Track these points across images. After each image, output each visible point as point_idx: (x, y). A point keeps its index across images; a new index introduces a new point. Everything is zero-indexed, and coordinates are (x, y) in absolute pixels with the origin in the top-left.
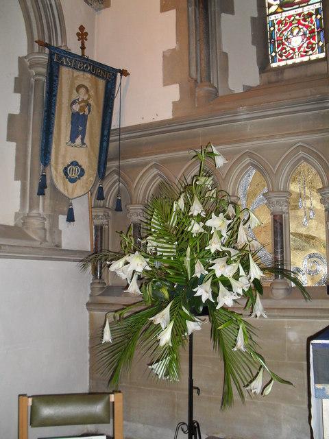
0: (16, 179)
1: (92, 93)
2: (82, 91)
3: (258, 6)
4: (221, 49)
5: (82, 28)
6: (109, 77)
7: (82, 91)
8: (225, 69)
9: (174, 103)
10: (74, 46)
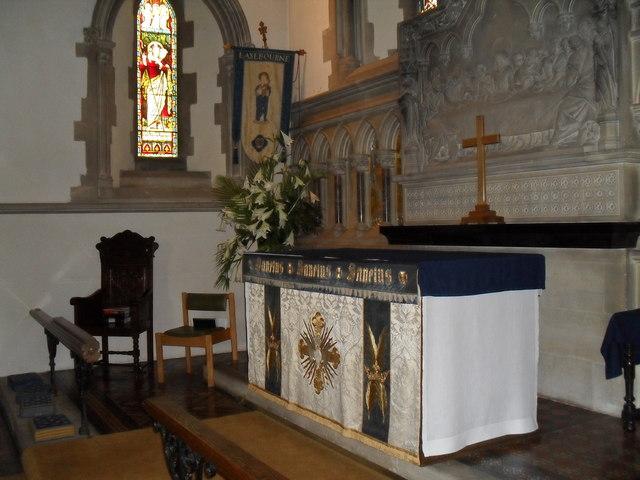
0: (222, 153)
1: (272, 77)
2: (264, 78)
3: (242, 13)
4: (366, 20)
5: (262, 24)
6: (288, 60)
7: (264, 78)
8: (371, 40)
9: (76, 124)
10: (257, 41)
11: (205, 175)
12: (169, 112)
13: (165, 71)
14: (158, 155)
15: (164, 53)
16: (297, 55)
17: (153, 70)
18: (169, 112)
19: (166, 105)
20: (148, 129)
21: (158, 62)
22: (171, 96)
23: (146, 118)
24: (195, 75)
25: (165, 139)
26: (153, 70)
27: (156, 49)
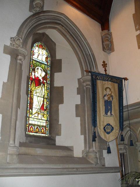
0: (81, 134)
1: (112, 90)
5: (104, 62)
7: (108, 90)
10: (101, 70)
11: (69, 149)
12: (45, 108)
13: (44, 85)
14: (38, 134)
15: (43, 74)
16: (123, 80)
17: (37, 82)
18: (45, 108)
19: (43, 104)
20: (33, 117)
21: (40, 78)
22: (46, 98)
23: (32, 110)
24: (62, 87)
25: (42, 124)
26: (37, 82)
27: (39, 71)
